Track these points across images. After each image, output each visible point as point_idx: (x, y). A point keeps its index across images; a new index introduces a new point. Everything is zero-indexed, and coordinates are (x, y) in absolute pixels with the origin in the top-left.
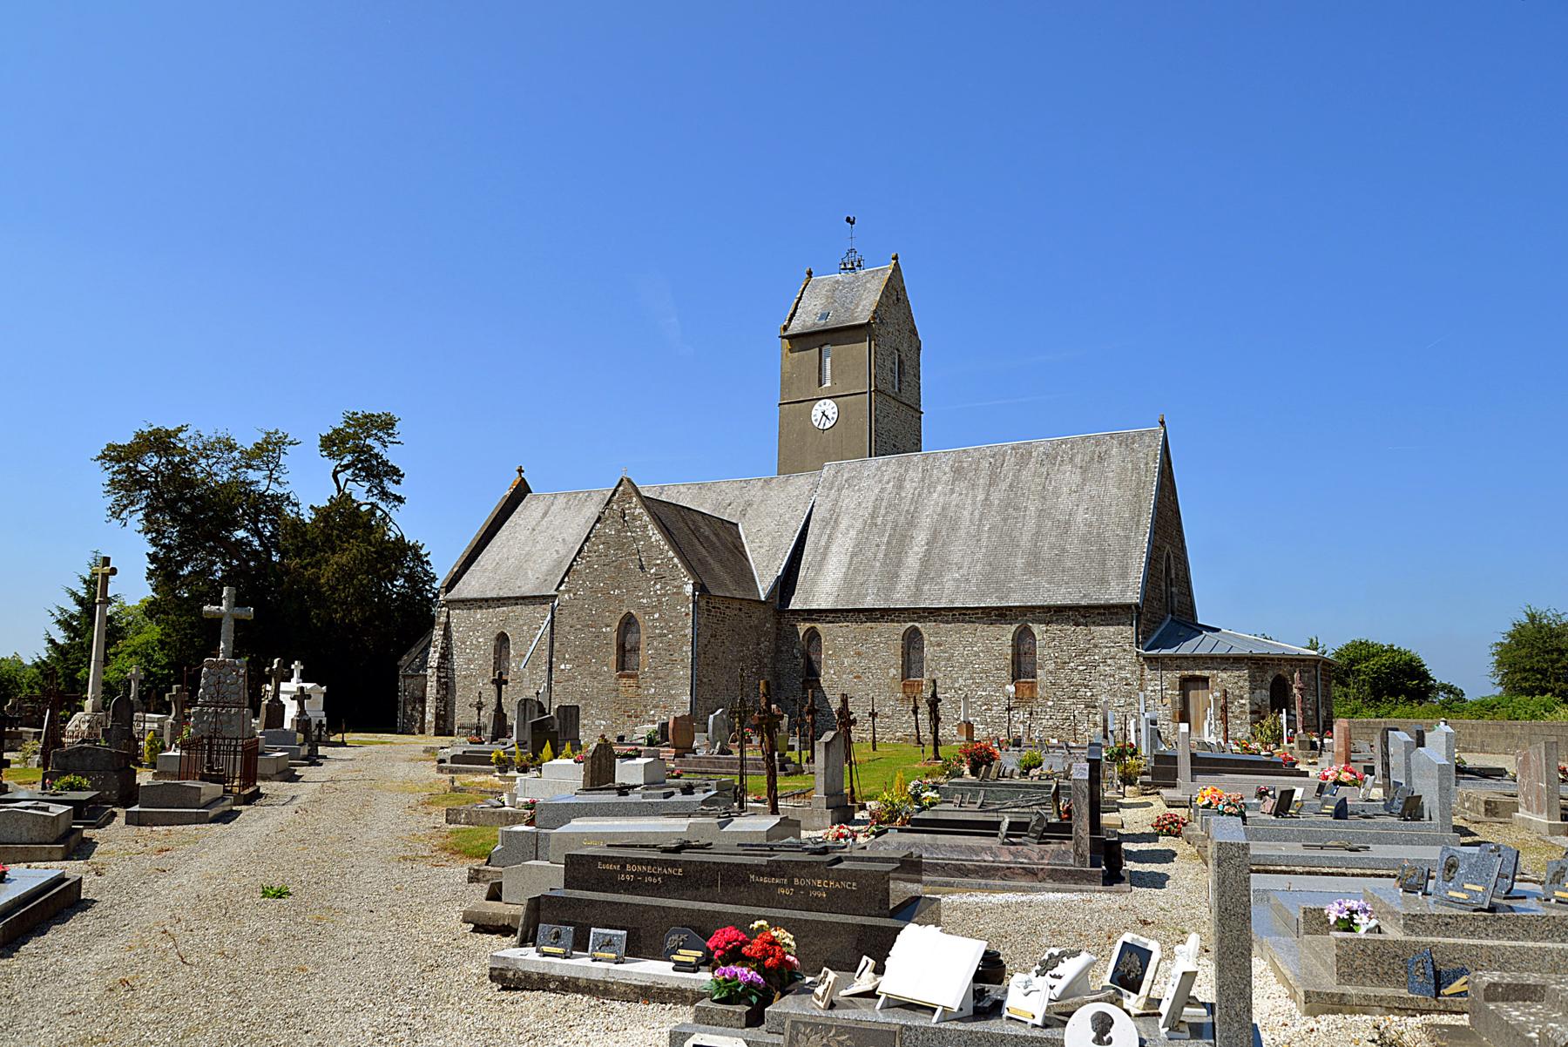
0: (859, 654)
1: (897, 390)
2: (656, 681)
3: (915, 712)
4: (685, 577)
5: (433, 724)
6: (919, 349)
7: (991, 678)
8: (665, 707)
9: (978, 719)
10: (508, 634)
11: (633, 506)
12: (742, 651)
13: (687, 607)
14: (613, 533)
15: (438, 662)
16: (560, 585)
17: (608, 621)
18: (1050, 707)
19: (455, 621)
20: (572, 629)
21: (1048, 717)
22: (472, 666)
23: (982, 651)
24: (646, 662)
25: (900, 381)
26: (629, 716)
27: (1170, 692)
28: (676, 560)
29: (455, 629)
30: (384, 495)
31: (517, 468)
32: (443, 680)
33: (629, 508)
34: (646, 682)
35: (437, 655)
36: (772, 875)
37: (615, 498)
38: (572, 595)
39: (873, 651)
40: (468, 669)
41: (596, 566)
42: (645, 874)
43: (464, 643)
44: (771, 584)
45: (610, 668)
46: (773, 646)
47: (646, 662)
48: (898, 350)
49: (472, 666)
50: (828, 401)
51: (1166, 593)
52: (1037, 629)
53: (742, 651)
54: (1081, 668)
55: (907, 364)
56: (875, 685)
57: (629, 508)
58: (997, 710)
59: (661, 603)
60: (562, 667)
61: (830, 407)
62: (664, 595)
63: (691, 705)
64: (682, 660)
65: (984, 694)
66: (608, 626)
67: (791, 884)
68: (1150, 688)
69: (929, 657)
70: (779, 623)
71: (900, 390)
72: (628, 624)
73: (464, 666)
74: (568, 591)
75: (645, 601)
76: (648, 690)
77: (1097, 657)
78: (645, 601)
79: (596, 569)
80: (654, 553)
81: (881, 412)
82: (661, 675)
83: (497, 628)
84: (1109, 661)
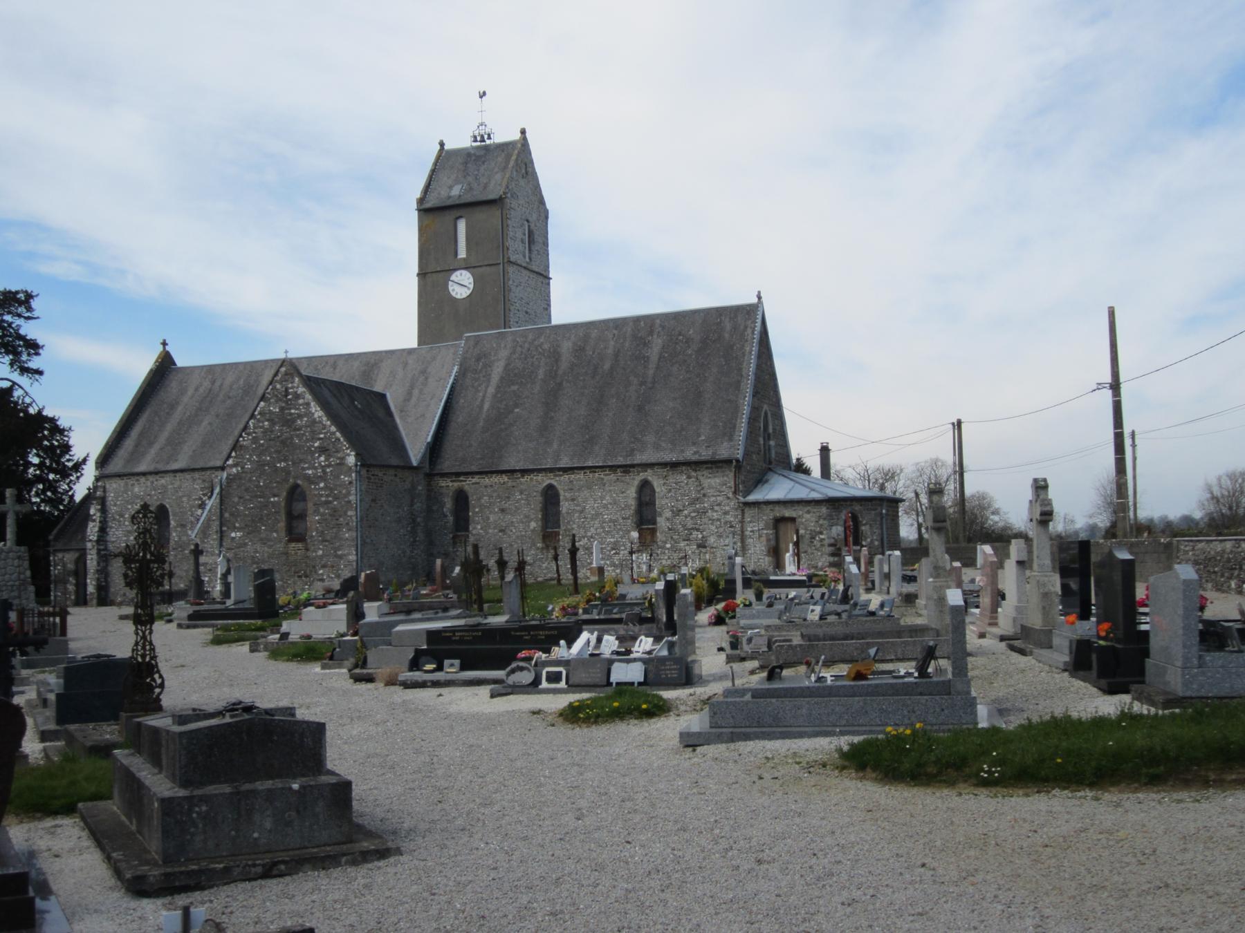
0: (503, 510)
1: (527, 260)
2: (324, 543)
3: (556, 558)
4: (347, 449)
5: (96, 595)
6: (547, 218)
7: (619, 527)
8: (333, 567)
9: (608, 562)
10: (168, 506)
11: (295, 385)
12: (398, 513)
13: (350, 476)
14: (277, 410)
15: (98, 536)
16: (227, 459)
17: (276, 491)
18: (668, 549)
20: (242, 500)
21: (666, 557)
23: (611, 504)
24: (314, 527)
25: (530, 250)
26: (300, 577)
27: (765, 532)
28: (338, 434)
29: (112, 503)
30: (24, 370)
31: (162, 341)
32: (103, 552)
33: (292, 388)
34: (314, 545)
35: (97, 529)
36: (521, 631)
37: (278, 378)
38: (239, 469)
39: (516, 507)
41: (262, 442)
42: (464, 636)
43: (122, 516)
44: (422, 451)
45: (279, 533)
46: (425, 506)
47: (314, 527)
48: (528, 221)
50: (464, 272)
51: (764, 447)
52: (658, 484)
53: (398, 513)
54: (693, 514)
55: (536, 233)
56: (518, 537)
57: (292, 388)
58: (624, 553)
59: (324, 472)
60: (233, 535)
62: (329, 466)
63: (357, 564)
64: (348, 524)
65: (612, 540)
66: (275, 496)
67: (529, 634)
68: (749, 529)
70: (429, 485)
71: (530, 259)
72: (295, 494)
74: (235, 465)
75: (310, 472)
76: (316, 552)
77: (706, 505)
78: (310, 472)
79: (262, 445)
80: (317, 427)
81: (514, 282)
82: (328, 538)
83: (156, 500)
84: (716, 508)
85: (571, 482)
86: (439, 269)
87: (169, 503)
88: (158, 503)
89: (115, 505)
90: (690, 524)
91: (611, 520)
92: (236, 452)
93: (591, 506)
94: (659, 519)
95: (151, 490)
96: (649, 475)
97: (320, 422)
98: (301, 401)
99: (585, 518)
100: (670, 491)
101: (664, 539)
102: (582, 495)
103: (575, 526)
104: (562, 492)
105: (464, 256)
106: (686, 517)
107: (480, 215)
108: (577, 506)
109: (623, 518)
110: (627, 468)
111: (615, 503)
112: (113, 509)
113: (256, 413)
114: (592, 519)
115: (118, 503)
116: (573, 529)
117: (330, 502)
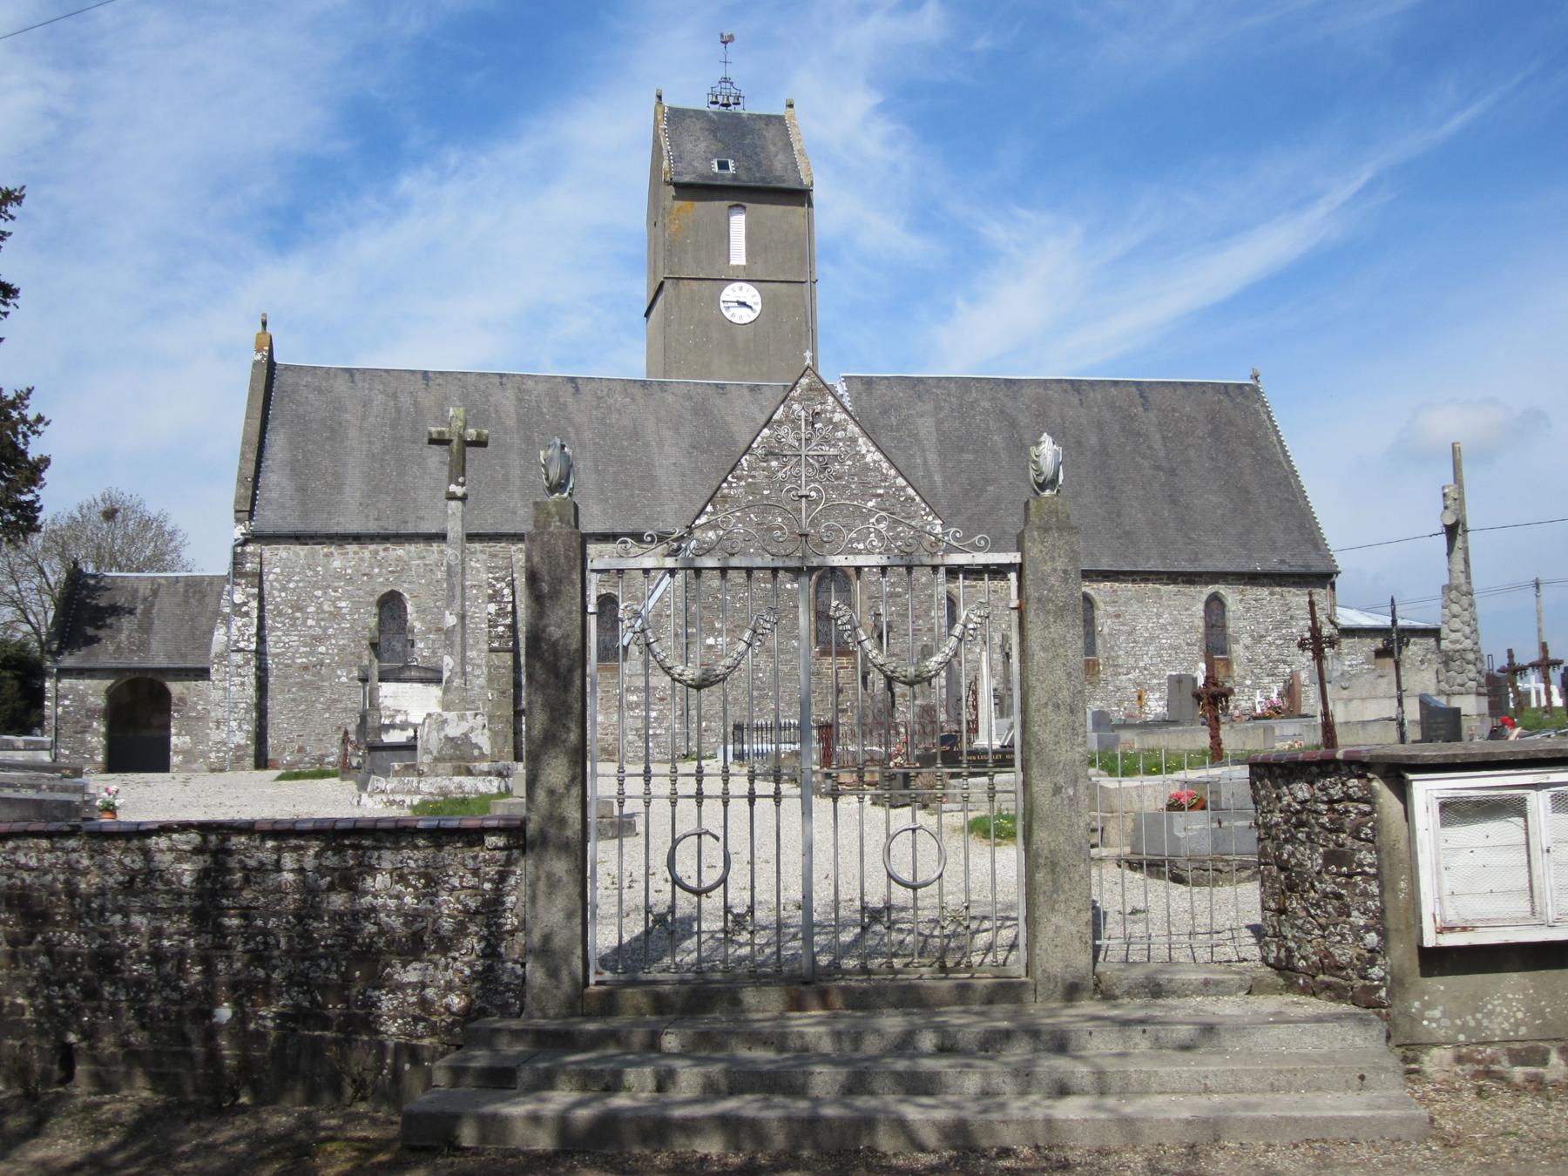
11: (829, 408)
16: (698, 517)
19: (278, 570)
22: (322, 649)
23: (1170, 624)
37: (795, 394)
40: (312, 653)
41: (766, 492)
49: (322, 649)
50: (746, 286)
60: (710, 641)
61: (749, 293)
69: (1106, 630)
73: (302, 649)
85: (1115, 591)
86: (701, 276)
87: (408, 590)
88: (387, 590)
89: (284, 589)
90: (1274, 654)
91: (1172, 647)
92: (714, 507)
93: (1143, 626)
94: (1235, 647)
95: (372, 566)
96: (1222, 589)
97: (878, 469)
98: (840, 434)
99: (1135, 642)
100: (1248, 610)
101: (1243, 673)
102: (1130, 610)
103: (1121, 653)
104: (1101, 605)
105: (743, 262)
106: (1270, 644)
107: (771, 212)
108: (1123, 625)
109: (1188, 644)
110: (1191, 578)
111: (1176, 623)
112: (275, 596)
113: (755, 445)
114: (1146, 644)
115: (292, 585)
116: (1118, 656)
117: (899, 595)
